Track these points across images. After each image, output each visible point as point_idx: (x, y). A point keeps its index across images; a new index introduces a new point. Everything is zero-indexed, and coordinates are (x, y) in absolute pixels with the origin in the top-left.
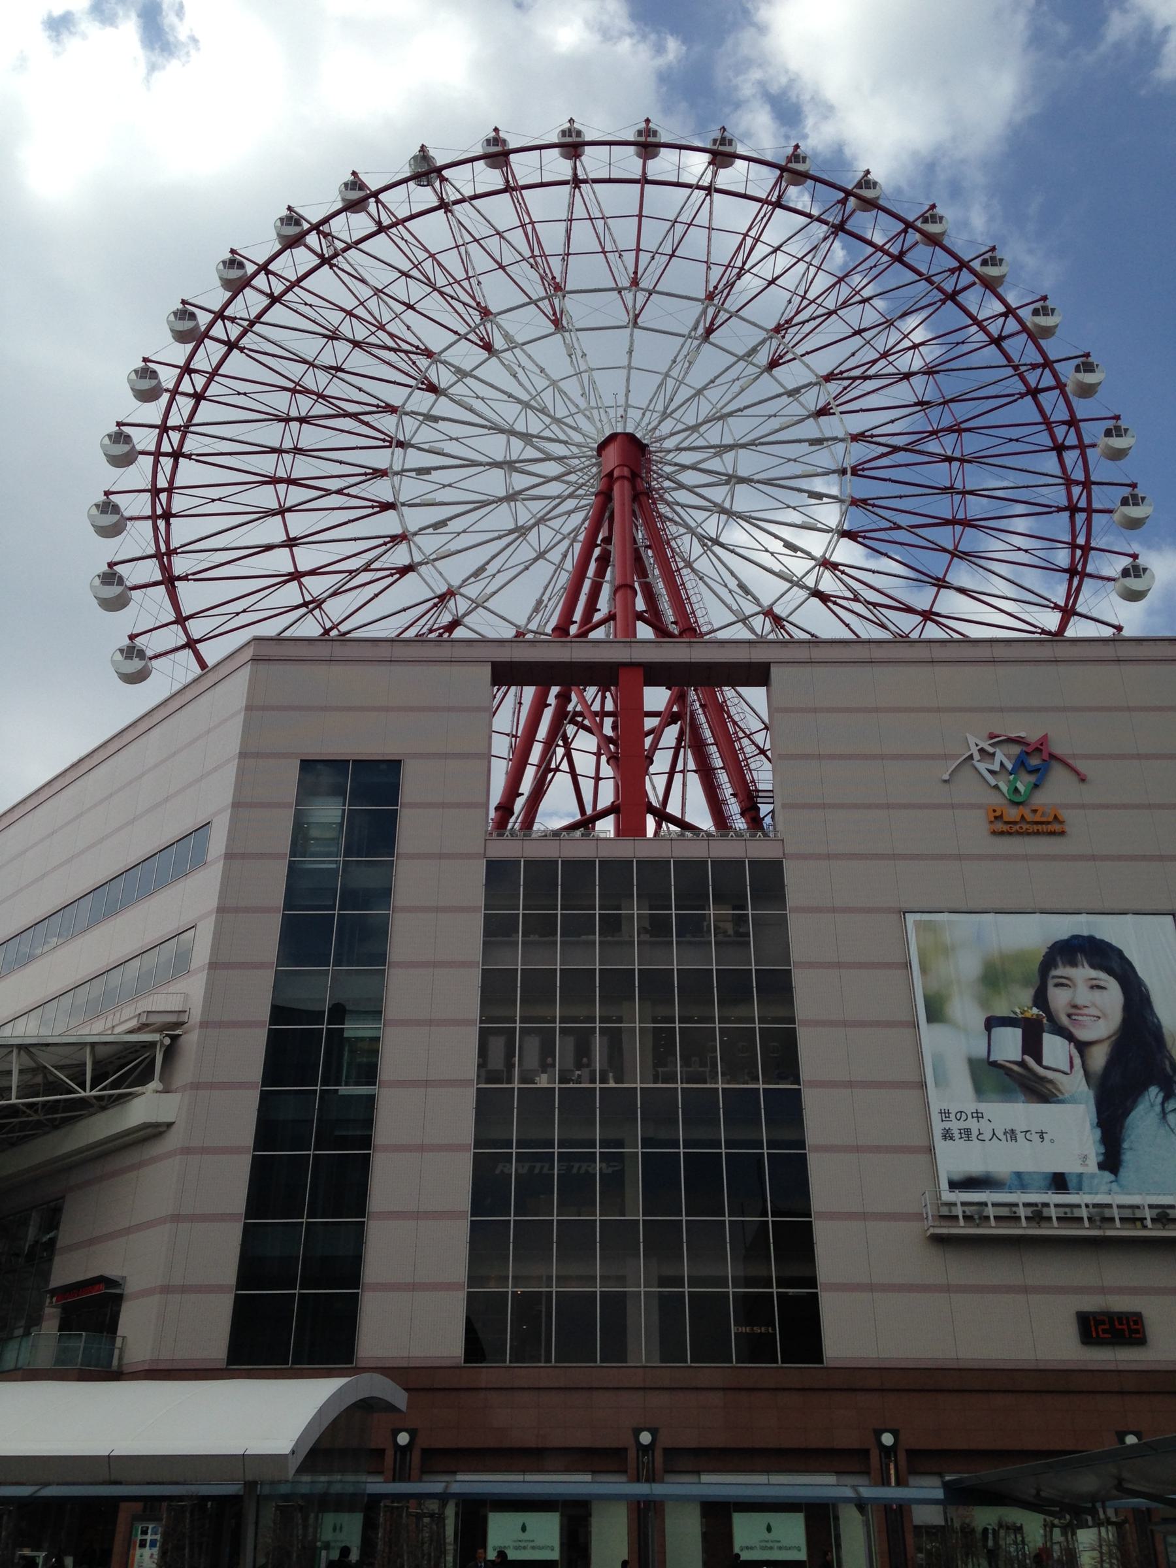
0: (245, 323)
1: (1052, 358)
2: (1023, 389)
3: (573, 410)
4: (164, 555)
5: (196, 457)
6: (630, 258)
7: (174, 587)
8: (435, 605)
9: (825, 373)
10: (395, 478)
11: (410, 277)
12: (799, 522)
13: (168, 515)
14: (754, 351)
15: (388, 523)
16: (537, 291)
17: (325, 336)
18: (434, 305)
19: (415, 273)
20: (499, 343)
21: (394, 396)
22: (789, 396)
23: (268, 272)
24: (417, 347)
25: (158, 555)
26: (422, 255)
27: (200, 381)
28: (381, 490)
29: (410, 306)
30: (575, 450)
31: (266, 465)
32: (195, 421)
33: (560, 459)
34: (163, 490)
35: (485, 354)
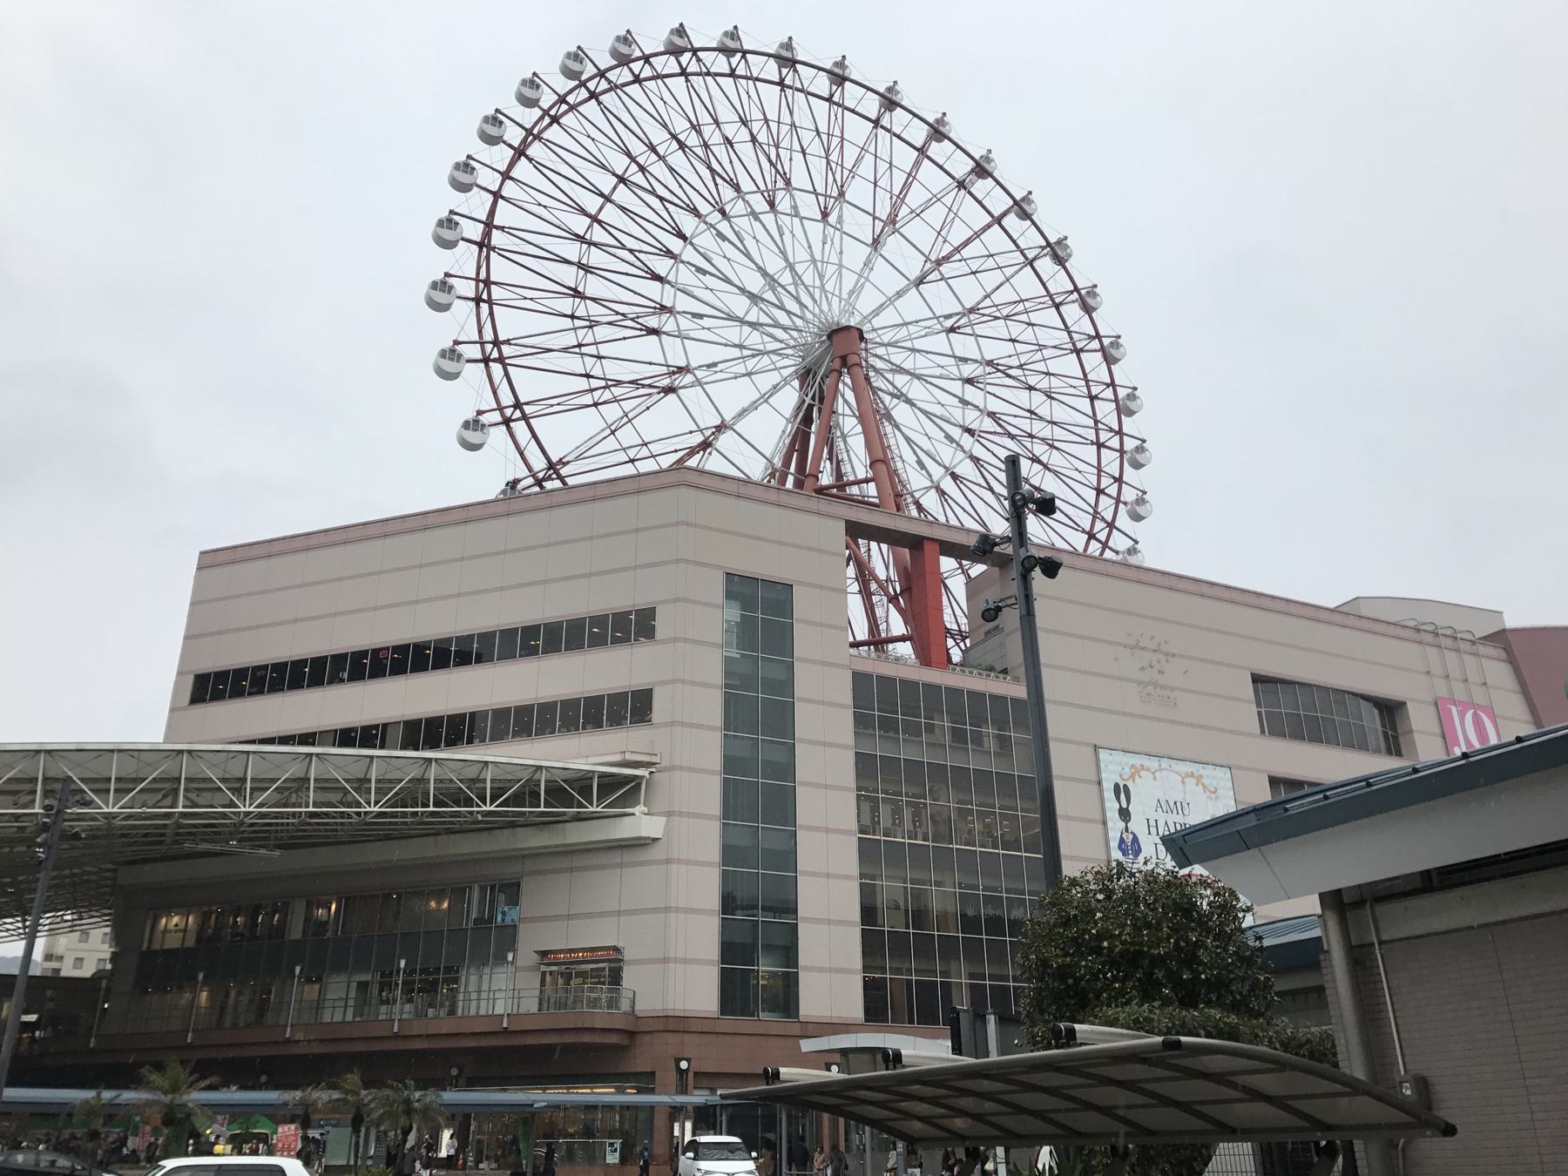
0: (704, 70)
2: (1088, 528)
3: (837, 292)
4: (532, 135)
5: (604, 109)
6: (947, 249)
7: (519, 158)
10: (702, 224)
11: (819, 136)
13: (555, 120)
14: (965, 360)
15: (675, 244)
16: (883, 212)
17: (740, 118)
18: (818, 165)
19: (825, 137)
20: (832, 219)
21: (746, 185)
22: (960, 402)
24: (785, 174)
25: (529, 132)
26: (837, 132)
27: (647, 72)
28: (688, 223)
29: (803, 152)
30: (817, 311)
31: (637, 148)
32: (625, 89)
33: (802, 305)
34: (567, 103)
35: (819, 217)
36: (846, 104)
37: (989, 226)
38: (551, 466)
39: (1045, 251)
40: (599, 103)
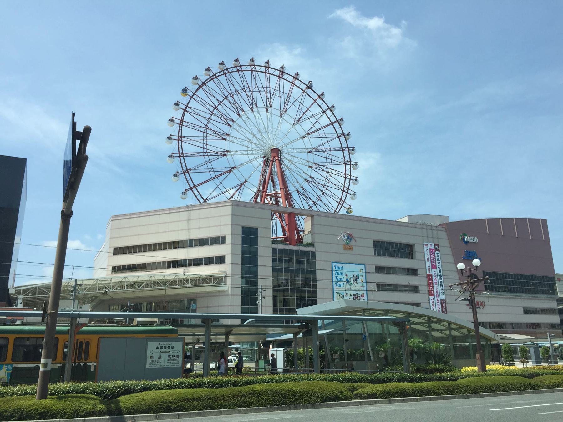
1: (349, 189)
8: (225, 134)
9: (311, 176)
12: (292, 183)
23: (268, 69)
29: (259, 91)
36: (243, 69)
37: (329, 125)
38: (187, 170)
39: (342, 135)
40: (226, 76)
